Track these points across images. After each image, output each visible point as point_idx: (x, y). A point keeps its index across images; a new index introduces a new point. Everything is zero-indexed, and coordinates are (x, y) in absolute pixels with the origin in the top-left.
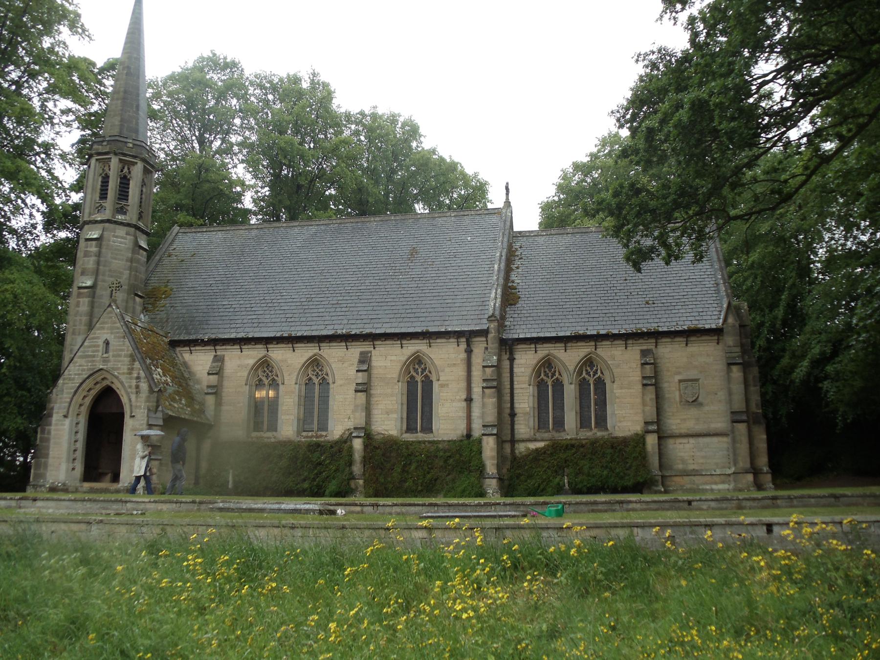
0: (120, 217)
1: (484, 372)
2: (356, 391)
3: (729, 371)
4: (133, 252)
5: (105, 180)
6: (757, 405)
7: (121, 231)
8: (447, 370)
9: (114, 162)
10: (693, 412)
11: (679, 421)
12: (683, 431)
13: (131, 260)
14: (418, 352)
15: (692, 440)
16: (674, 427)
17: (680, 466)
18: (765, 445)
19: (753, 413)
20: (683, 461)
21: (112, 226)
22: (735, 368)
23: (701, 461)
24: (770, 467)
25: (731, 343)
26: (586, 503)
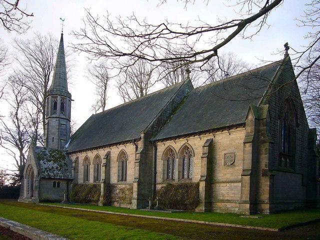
0: (53, 116)
1: (203, 149)
2: (202, 158)
3: (245, 146)
4: (59, 126)
5: (56, 104)
6: (266, 165)
7: (54, 120)
8: (131, 156)
9: (59, 98)
10: (230, 170)
11: (222, 175)
12: (224, 180)
13: (59, 129)
14: (185, 144)
15: (228, 185)
16: (220, 178)
17: (221, 198)
18: (268, 188)
19: (263, 170)
20: (223, 196)
21: (51, 119)
22: (247, 145)
23: (233, 195)
24: (270, 201)
25: (249, 131)
26: (178, 212)
